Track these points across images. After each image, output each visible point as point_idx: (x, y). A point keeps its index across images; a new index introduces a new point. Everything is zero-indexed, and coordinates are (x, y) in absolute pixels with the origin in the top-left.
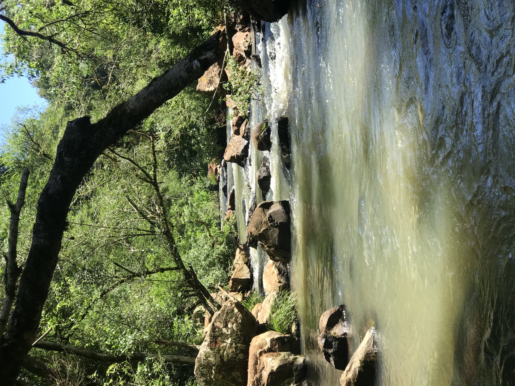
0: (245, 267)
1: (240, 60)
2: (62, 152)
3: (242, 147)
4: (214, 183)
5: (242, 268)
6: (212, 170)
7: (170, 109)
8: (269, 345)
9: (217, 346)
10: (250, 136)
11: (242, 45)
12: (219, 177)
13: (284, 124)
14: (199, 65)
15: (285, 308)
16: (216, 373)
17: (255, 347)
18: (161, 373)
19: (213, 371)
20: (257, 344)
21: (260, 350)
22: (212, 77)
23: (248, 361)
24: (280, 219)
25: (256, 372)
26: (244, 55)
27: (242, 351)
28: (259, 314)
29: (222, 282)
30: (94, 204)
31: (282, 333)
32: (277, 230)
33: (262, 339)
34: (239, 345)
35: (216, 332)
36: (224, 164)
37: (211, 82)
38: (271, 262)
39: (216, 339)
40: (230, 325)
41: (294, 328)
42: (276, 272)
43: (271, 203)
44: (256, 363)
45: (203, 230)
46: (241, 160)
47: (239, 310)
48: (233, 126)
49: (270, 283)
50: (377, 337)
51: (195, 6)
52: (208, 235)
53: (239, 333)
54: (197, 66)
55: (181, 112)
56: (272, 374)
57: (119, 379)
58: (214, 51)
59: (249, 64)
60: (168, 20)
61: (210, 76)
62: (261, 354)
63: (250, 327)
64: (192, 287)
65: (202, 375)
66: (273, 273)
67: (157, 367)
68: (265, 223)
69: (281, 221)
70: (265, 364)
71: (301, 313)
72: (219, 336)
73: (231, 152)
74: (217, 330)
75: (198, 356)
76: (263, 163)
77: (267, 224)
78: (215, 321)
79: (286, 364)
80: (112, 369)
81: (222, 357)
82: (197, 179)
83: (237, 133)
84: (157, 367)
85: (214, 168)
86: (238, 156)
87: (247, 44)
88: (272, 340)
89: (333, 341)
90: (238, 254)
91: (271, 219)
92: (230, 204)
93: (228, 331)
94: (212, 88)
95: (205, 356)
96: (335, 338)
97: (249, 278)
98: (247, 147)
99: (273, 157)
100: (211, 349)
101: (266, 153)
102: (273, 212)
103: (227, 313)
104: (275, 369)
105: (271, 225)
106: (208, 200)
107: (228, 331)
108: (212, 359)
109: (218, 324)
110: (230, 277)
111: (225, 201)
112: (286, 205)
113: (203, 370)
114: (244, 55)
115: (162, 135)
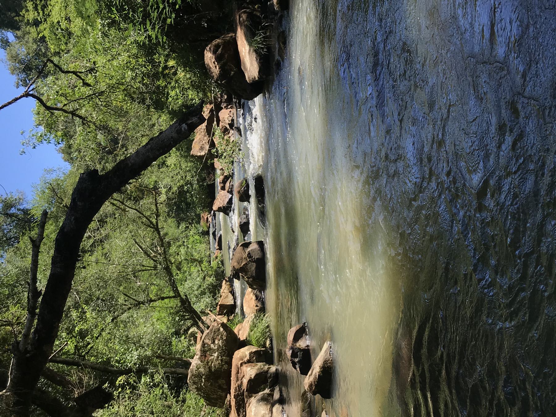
0: (230, 295)
1: (225, 131)
3: (227, 200)
4: (206, 229)
7: (170, 170)
8: (248, 357)
9: (206, 359)
13: (259, 181)
15: (261, 326)
18: (161, 383)
21: (241, 362)
22: (203, 144)
24: (256, 256)
25: (237, 380)
26: (228, 127)
27: (226, 363)
28: (240, 332)
30: (107, 246)
31: (259, 347)
33: (242, 352)
34: (224, 358)
37: (202, 148)
38: (250, 290)
40: (216, 342)
42: (254, 298)
43: (250, 243)
49: (249, 306)
51: (189, 88)
56: (250, 381)
59: (233, 134)
60: (167, 99)
62: (241, 365)
63: (233, 343)
64: (187, 311)
65: (194, 383)
66: (252, 299)
67: (158, 378)
69: (258, 257)
74: (206, 345)
75: (191, 367)
76: (244, 212)
78: (205, 339)
80: (121, 380)
81: (210, 368)
83: (223, 188)
84: (158, 378)
85: (206, 218)
86: (224, 207)
87: (230, 118)
90: (225, 286)
91: (249, 255)
98: (231, 199)
99: (252, 207)
100: (201, 361)
101: (246, 203)
106: (200, 243)
108: (202, 370)
109: (207, 341)
112: (261, 244)
115: (164, 191)
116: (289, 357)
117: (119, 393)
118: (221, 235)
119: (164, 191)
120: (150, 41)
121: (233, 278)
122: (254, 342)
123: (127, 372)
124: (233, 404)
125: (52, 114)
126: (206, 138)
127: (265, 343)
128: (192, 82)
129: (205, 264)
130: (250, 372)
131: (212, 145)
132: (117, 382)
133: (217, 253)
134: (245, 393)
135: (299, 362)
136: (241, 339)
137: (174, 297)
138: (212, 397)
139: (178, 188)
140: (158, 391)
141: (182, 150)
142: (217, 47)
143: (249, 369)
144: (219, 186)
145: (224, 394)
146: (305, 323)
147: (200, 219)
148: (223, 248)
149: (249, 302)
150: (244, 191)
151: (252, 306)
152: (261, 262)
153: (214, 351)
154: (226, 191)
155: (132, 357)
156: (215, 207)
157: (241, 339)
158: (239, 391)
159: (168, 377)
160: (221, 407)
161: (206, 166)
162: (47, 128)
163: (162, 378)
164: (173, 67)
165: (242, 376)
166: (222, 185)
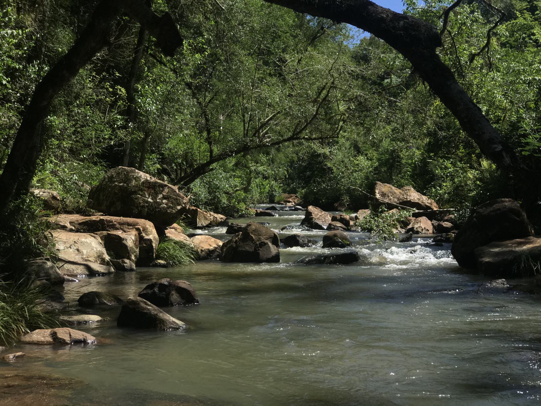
0: (207, 222)
1: (404, 224)
2: (408, 20)
3: (320, 223)
4: (276, 199)
5: (207, 219)
6: (289, 198)
7: (352, 159)
8: (146, 237)
9: (146, 189)
10: (331, 230)
11: (419, 225)
12: (282, 204)
13: (352, 259)
14: (497, 150)
15: (181, 254)
16: (120, 186)
17: (144, 224)
18: (116, 137)
19: (122, 184)
20: (147, 226)
21: (141, 229)
22: (388, 197)
23: (130, 217)
24: (262, 253)
25: (120, 224)
26: (410, 226)
27: (140, 212)
28: (173, 230)
29: (194, 199)
30: (274, 80)
31: (157, 251)
32: (252, 250)
33: (152, 231)
34: (146, 210)
35: (159, 188)
36: (298, 208)
37: (383, 195)
38: (221, 244)
39: (152, 188)
40: (164, 201)
41: (162, 262)
42: (211, 248)
43: (277, 246)
44: (129, 224)
45: (242, 184)
46: (309, 222)
47: (179, 210)
48: (341, 215)
49: (201, 242)
50: (179, 332)
51: (454, 183)
52: (238, 188)
53: (157, 210)
54: (496, 148)
55: (348, 169)
56: (120, 239)
57: (112, 97)
58: (512, 165)
59: (400, 232)
60: (441, 158)
61: (389, 195)
62: (138, 229)
63: (162, 222)
64: (188, 172)
65: (118, 174)
66: (210, 245)
67: (121, 134)
68: (259, 238)
69: (261, 254)
70: (129, 233)
71: (177, 270)
72: (155, 190)
73: (316, 213)
74: (161, 189)
75: (137, 171)
76: (311, 241)
77: (258, 241)
78: (169, 187)
79: (129, 253)
80: (123, 91)
81: (135, 193)
82: (280, 183)
83: (334, 219)
84: (121, 134)
85: (291, 200)
86: (312, 218)
87: (420, 230)
88: (150, 240)
89: (166, 292)
90: (220, 217)
91: (263, 244)
92: (261, 212)
93: (159, 199)
94: (378, 196)
95: (137, 177)
96: (168, 294)
97: (198, 225)
98: (320, 227)
99: (318, 249)
100: (143, 183)
101: (321, 243)
102: (269, 247)
103: (177, 199)
104: (124, 242)
105: (257, 244)
106: (261, 193)
107: (159, 199)
108: (134, 183)
109: (166, 190)
110: (199, 208)
111: (263, 208)
112: (275, 259)
113: (123, 174)
114: (410, 226)
115: (327, 151)
116: (160, 281)
117: (107, 89)
118: (273, 216)
119: (327, 151)
120: (521, 136)
121: (228, 226)
122: (163, 245)
123: (131, 99)
124: (94, 218)
125: (439, 17)
126: (396, 200)
127: (162, 258)
128: (463, 186)
129: (243, 194)
130: (130, 239)
131: (390, 207)
132: (119, 87)
133: (253, 211)
134: (105, 233)
135: (154, 292)
136: (166, 231)
137: (211, 156)
138: (101, 195)
139: (329, 168)
140: (107, 133)
141: (375, 174)
142: (519, 215)
143: (133, 238)
144: (337, 214)
145: (104, 208)
146: (198, 302)
147: (289, 193)
148: (258, 217)
149: (204, 241)
150: (338, 242)
151: (202, 245)
152: (254, 258)
153: (154, 198)
154: (330, 222)
155: (149, 104)
156: (311, 208)
157: (166, 231)
158: (108, 226)
159: (121, 145)
160: (88, 204)
161: (364, 199)
162: (422, 11)
163: (121, 139)
164: (480, 165)
165: (126, 229)
166: (338, 217)
